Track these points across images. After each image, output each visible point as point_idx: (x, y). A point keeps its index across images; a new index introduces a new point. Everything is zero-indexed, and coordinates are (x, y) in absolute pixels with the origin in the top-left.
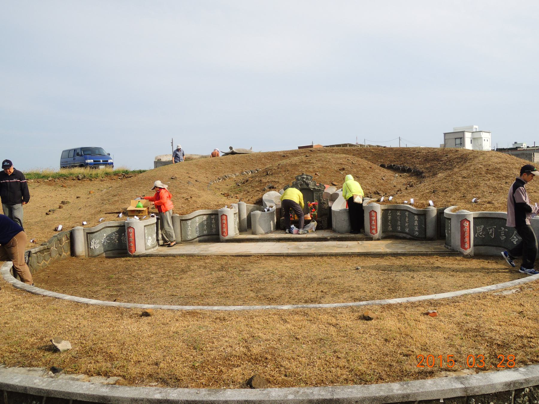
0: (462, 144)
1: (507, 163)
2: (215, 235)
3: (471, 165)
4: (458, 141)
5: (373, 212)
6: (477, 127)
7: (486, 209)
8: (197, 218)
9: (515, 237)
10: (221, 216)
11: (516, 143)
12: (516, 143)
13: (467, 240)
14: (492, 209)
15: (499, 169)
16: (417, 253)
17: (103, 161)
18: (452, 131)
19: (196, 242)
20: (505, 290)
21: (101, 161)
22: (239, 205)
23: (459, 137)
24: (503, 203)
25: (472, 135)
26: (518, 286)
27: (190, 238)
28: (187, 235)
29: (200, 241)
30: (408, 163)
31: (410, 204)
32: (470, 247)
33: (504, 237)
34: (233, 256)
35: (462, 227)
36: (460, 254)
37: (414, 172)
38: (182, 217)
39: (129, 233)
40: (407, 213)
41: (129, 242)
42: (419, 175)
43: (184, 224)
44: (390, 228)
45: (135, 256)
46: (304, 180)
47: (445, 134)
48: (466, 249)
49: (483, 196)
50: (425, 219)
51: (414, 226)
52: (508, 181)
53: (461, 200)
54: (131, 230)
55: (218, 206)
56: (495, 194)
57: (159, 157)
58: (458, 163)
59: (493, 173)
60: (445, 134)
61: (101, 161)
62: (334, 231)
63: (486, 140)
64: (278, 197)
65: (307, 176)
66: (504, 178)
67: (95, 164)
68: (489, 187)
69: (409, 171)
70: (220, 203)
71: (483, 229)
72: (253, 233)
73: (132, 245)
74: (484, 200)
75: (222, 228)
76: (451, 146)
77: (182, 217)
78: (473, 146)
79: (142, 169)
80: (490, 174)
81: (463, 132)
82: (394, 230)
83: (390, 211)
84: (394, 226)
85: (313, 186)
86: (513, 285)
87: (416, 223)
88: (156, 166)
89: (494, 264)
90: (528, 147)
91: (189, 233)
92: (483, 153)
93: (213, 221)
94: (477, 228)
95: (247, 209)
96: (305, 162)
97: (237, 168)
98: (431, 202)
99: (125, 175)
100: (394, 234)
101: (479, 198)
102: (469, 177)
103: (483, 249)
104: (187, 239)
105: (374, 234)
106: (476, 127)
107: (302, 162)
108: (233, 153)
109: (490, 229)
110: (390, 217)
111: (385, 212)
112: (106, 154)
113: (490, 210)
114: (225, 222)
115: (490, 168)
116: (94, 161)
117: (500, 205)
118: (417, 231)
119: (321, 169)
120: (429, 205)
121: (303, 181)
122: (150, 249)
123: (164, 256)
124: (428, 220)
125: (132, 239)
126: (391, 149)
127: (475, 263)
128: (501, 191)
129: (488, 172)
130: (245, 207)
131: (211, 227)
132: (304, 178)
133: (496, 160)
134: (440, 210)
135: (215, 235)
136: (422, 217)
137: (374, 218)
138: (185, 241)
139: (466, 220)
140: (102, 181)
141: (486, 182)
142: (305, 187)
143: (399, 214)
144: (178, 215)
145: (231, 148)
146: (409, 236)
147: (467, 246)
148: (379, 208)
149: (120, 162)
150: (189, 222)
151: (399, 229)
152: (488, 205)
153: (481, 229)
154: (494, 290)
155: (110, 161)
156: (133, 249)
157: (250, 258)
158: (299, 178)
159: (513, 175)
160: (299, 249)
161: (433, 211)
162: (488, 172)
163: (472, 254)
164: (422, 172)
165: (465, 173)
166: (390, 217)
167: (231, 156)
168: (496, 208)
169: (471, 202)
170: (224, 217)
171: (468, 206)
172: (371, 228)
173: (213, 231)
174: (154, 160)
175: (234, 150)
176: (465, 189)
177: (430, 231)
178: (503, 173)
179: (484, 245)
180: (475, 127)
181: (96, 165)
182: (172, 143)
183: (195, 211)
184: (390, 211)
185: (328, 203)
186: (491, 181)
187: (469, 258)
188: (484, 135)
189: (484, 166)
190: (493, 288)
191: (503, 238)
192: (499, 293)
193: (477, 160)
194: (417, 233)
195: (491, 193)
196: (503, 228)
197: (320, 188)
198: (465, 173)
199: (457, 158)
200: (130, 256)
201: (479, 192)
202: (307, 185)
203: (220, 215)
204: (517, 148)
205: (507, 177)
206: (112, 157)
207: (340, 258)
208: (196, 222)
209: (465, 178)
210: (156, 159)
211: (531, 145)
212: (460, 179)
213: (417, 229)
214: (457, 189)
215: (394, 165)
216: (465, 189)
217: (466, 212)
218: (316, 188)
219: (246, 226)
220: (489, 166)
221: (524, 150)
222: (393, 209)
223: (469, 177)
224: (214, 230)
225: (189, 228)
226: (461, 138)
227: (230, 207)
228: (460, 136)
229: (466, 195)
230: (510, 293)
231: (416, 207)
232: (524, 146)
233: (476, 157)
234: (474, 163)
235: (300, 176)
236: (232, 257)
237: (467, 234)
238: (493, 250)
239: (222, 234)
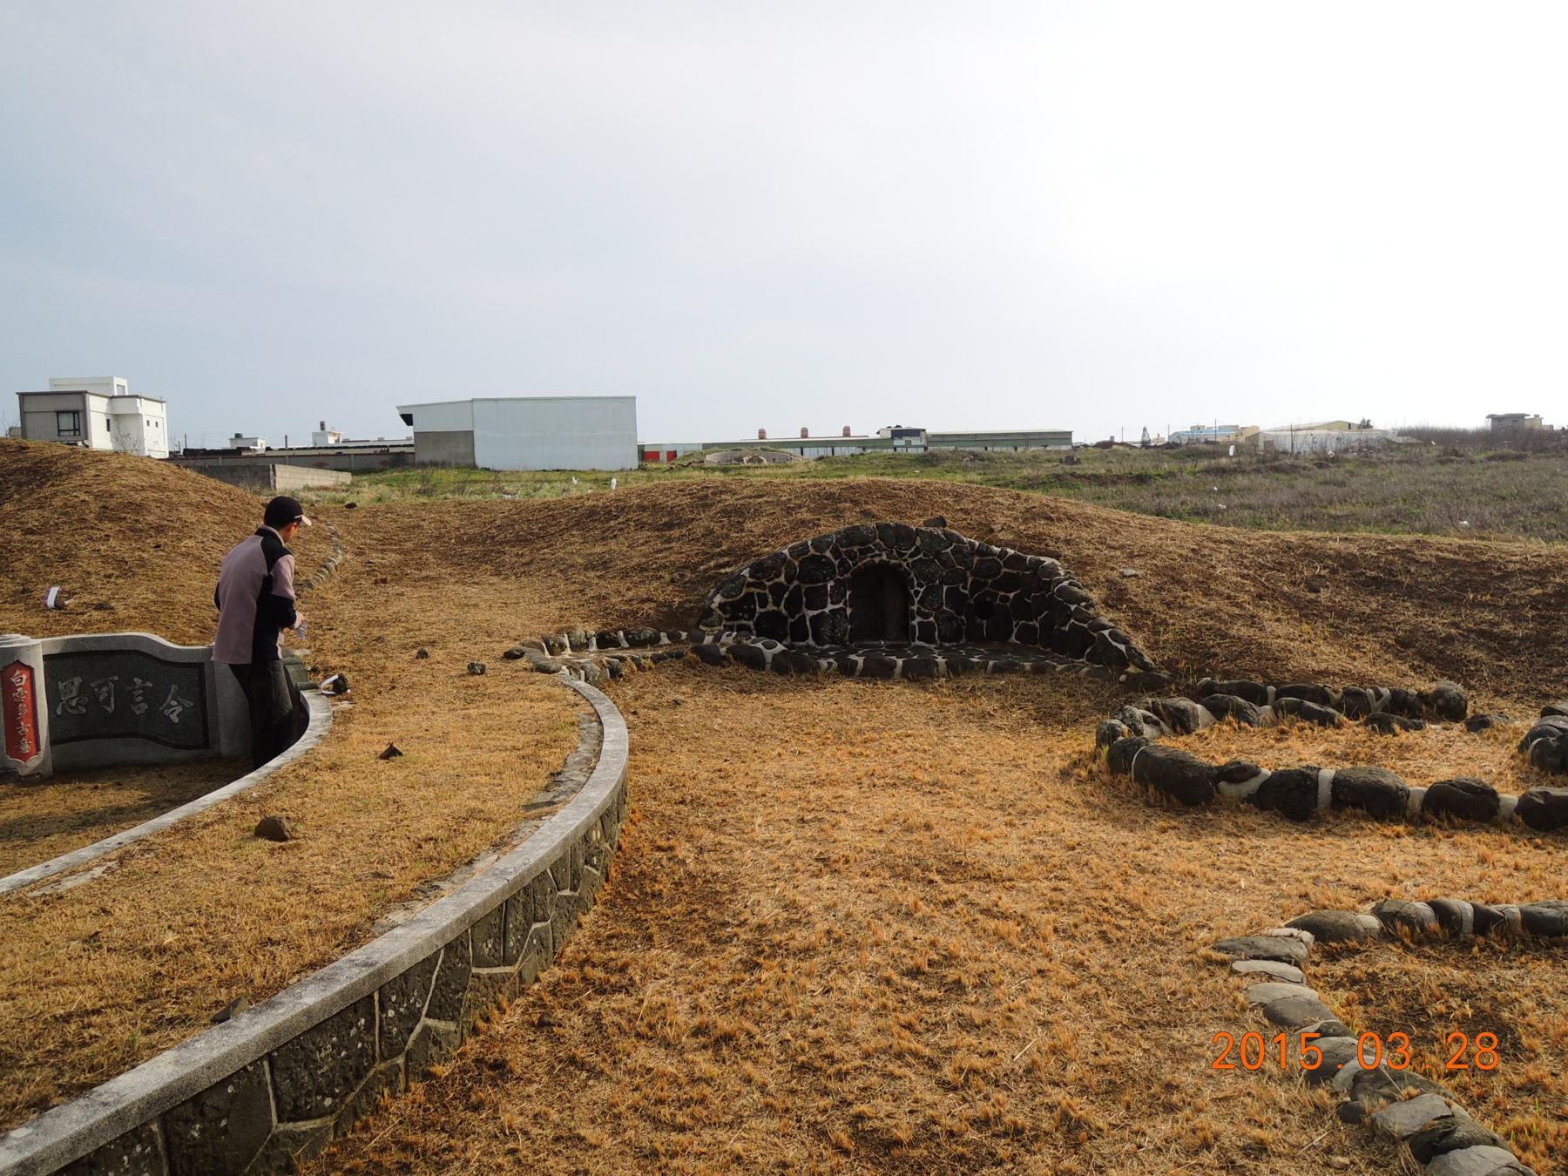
1: (166, 489)
3: (55, 495)
4: (67, 421)
6: (124, 382)
7: (86, 626)
9: (174, 703)
11: (238, 436)
12: (238, 436)
13: (26, 727)
14: (105, 626)
15: (139, 508)
20: (72, 873)
23: (68, 409)
24: (142, 605)
25: (110, 404)
26: (114, 855)
32: (38, 749)
33: (145, 706)
47: (23, 396)
48: (25, 757)
49: (84, 588)
52: (162, 541)
53: (14, 602)
56: (121, 581)
58: (20, 485)
59: (121, 519)
60: (23, 396)
63: (153, 424)
66: (152, 532)
68: (105, 559)
71: (80, 688)
74: (87, 598)
76: (44, 442)
78: (116, 439)
80: (111, 520)
81: (82, 395)
86: (99, 853)
89: (111, 791)
90: (268, 449)
92: (144, 466)
94: (61, 686)
101: (71, 594)
102: (44, 529)
103: (83, 751)
106: (120, 383)
109: (100, 687)
113: (99, 630)
115: (113, 503)
117: (132, 613)
127: (52, 801)
128: (141, 571)
129: (105, 514)
133: (133, 481)
141: (98, 546)
147: (27, 747)
152: (96, 615)
153: (75, 689)
154: (33, 882)
159: (177, 525)
162: (105, 514)
163: (49, 767)
165: (33, 518)
168: (118, 623)
171: (33, 621)
176: (30, 569)
178: (150, 518)
179: (87, 738)
180: (117, 381)
186: (113, 543)
187: (35, 784)
188: (147, 409)
189: (96, 497)
190: (31, 877)
191: (141, 708)
192: (48, 891)
193: (76, 480)
195: (110, 576)
196: (138, 681)
198: (33, 518)
199: (21, 471)
201: (74, 575)
204: (240, 450)
205: (160, 529)
209: (32, 532)
211: (277, 445)
212: (17, 536)
216: (30, 569)
217: (18, 640)
220: (111, 496)
221: (258, 456)
223: (44, 529)
226: (75, 413)
228: (73, 404)
229: (31, 586)
230: (83, 879)
232: (260, 447)
233: (79, 468)
234: (67, 486)
237: (24, 710)
238: (116, 749)
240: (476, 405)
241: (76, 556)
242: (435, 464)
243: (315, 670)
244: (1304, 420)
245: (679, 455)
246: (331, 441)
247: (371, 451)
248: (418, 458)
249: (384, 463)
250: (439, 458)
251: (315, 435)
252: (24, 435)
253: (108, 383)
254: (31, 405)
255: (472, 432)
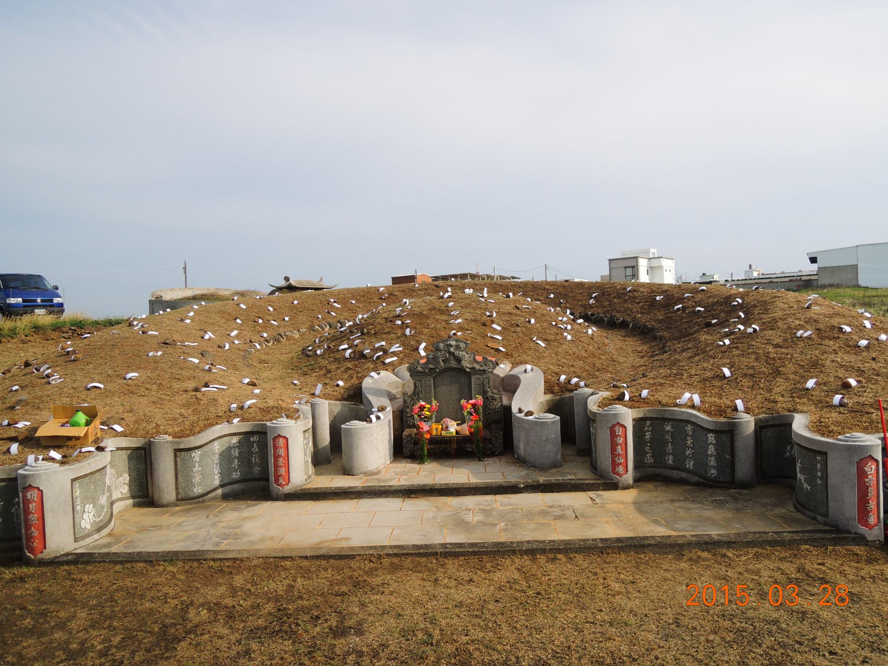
0: (635, 275)
2: (259, 479)
4: (629, 272)
5: (615, 426)
6: (654, 251)
8: (219, 438)
10: (275, 439)
11: (704, 274)
12: (704, 274)
13: (872, 505)
16: (750, 538)
17: (42, 301)
18: (621, 257)
19: (213, 499)
21: (39, 300)
22: (313, 406)
23: (630, 265)
25: (649, 262)
27: (198, 490)
28: (190, 483)
29: (225, 497)
30: (618, 312)
31: (693, 407)
34: (306, 558)
35: (862, 474)
36: (860, 540)
37: (635, 327)
38: (179, 443)
39: (27, 502)
40: (689, 428)
41: (28, 526)
42: (647, 333)
43: (183, 460)
44: (649, 459)
45: (42, 563)
46: (452, 350)
47: (610, 260)
50: (732, 441)
51: (707, 455)
54: (32, 495)
55: (265, 411)
57: (159, 293)
61: (39, 300)
62: (522, 462)
64: (393, 383)
65: (457, 341)
67: (25, 306)
69: (623, 325)
70: (271, 403)
72: (347, 471)
73: (36, 533)
75: (277, 467)
76: (619, 279)
77: (179, 443)
78: (651, 278)
79: (114, 315)
81: (636, 258)
82: (659, 461)
83: (648, 423)
84: (659, 454)
85: (470, 362)
87: (711, 450)
88: (152, 312)
91: (197, 479)
93: (255, 449)
95: (331, 412)
96: (439, 310)
97: (302, 318)
98: (739, 403)
99: (78, 327)
100: (658, 471)
104: (192, 494)
105: (620, 475)
106: (653, 251)
107: (434, 308)
108: (291, 288)
110: (648, 436)
111: (639, 423)
112: (50, 287)
114: (282, 452)
116: (24, 301)
118: (714, 467)
119: (473, 325)
120: (736, 409)
121: (450, 353)
122: (89, 535)
123: (121, 563)
124: (739, 444)
125: (34, 517)
126: (581, 285)
130: (327, 409)
131: (249, 461)
132: (451, 346)
134: (760, 420)
135: (259, 479)
136: (725, 438)
137: (620, 440)
138: (189, 500)
139: (871, 458)
140: (23, 342)
142: (453, 364)
143: (669, 428)
144: (170, 438)
145: (287, 279)
146: (694, 479)
147: (872, 520)
148: (627, 415)
149: (76, 306)
150: (196, 455)
151: (670, 460)
155: (56, 300)
156: (36, 544)
157: (353, 564)
158: (441, 345)
160: (460, 523)
161: (748, 422)
164: (653, 329)
166: (648, 436)
167: (289, 295)
169: (831, 406)
170: (281, 442)
172: (613, 462)
173: (255, 475)
174: (150, 298)
175: (293, 282)
177: (744, 466)
180: (652, 250)
181: (29, 307)
182: (185, 268)
183: (212, 425)
184: (648, 423)
185: (501, 399)
194: (713, 471)
197: (485, 368)
200: (29, 563)
202: (459, 360)
203: (270, 437)
206: (61, 295)
207: (579, 558)
208: (214, 454)
210: (153, 296)
213: (712, 462)
214: (777, 373)
215: (592, 315)
218: (477, 367)
219: (333, 453)
222: (656, 419)
224: (256, 469)
225: (197, 468)
226: (633, 267)
227: (293, 414)
228: (632, 263)
231: (709, 414)
235: (443, 342)
236: (306, 563)
239: (277, 480)
240: (859, 249)
241: (823, 366)
242: (831, 286)
243: (174, 639)
244: (387, 438)
245: (419, 280)
246: (755, 274)
247: (787, 279)
248: (820, 283)
249: (799, 286)
250: (835, 282)
251: (746, 272)
252: (610, 279)
253: (648, 252)
254: (614, 265)
255: (855, 267)
